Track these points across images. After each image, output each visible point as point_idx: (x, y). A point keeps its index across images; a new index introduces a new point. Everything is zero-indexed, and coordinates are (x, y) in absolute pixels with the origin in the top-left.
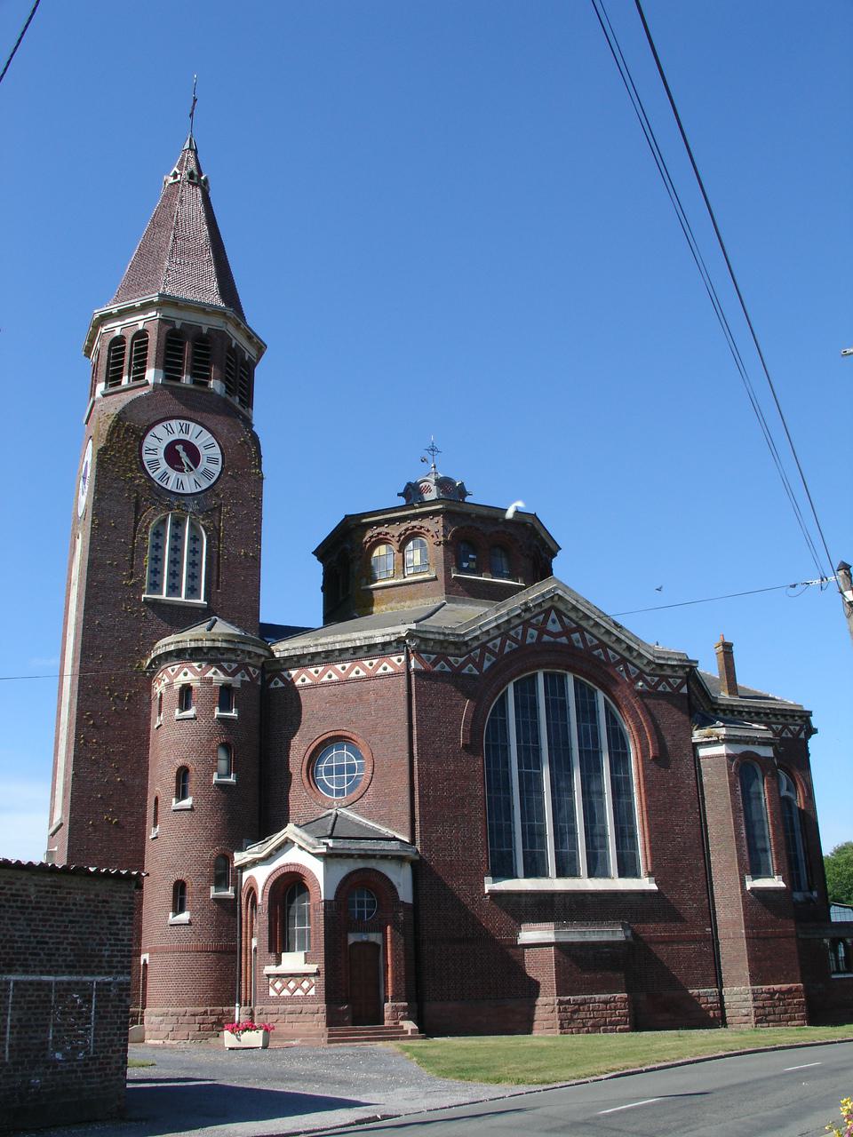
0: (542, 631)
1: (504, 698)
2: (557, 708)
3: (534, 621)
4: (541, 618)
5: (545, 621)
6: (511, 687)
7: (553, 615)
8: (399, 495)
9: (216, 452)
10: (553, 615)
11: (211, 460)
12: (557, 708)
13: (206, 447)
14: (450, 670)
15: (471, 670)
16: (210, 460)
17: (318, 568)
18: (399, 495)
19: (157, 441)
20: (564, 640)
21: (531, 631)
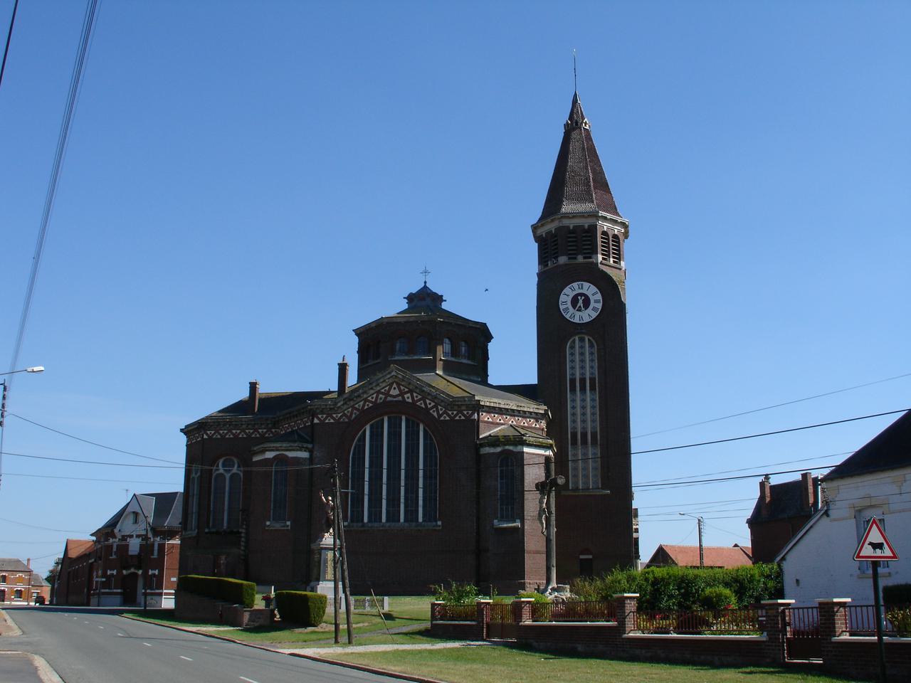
0: (387, 394)
1: (365, 430)
2: (394, 435)
3: (383, 391)
4: (387, 388)
5: (390, 389)
6: (368, 428)
7: (395, 385)
8: (404, 298)
9: (599, 297)
10: (395, 385)
11: (596, 301)
12: (394, 435)
13: (593, 295)
14: (318, 422)
15: (421, 404)
16: (596, 301)
17: (356, 339)
18: (404, 298)
19: (590, 290)
20: (400, 398)
21: (381, 396)
